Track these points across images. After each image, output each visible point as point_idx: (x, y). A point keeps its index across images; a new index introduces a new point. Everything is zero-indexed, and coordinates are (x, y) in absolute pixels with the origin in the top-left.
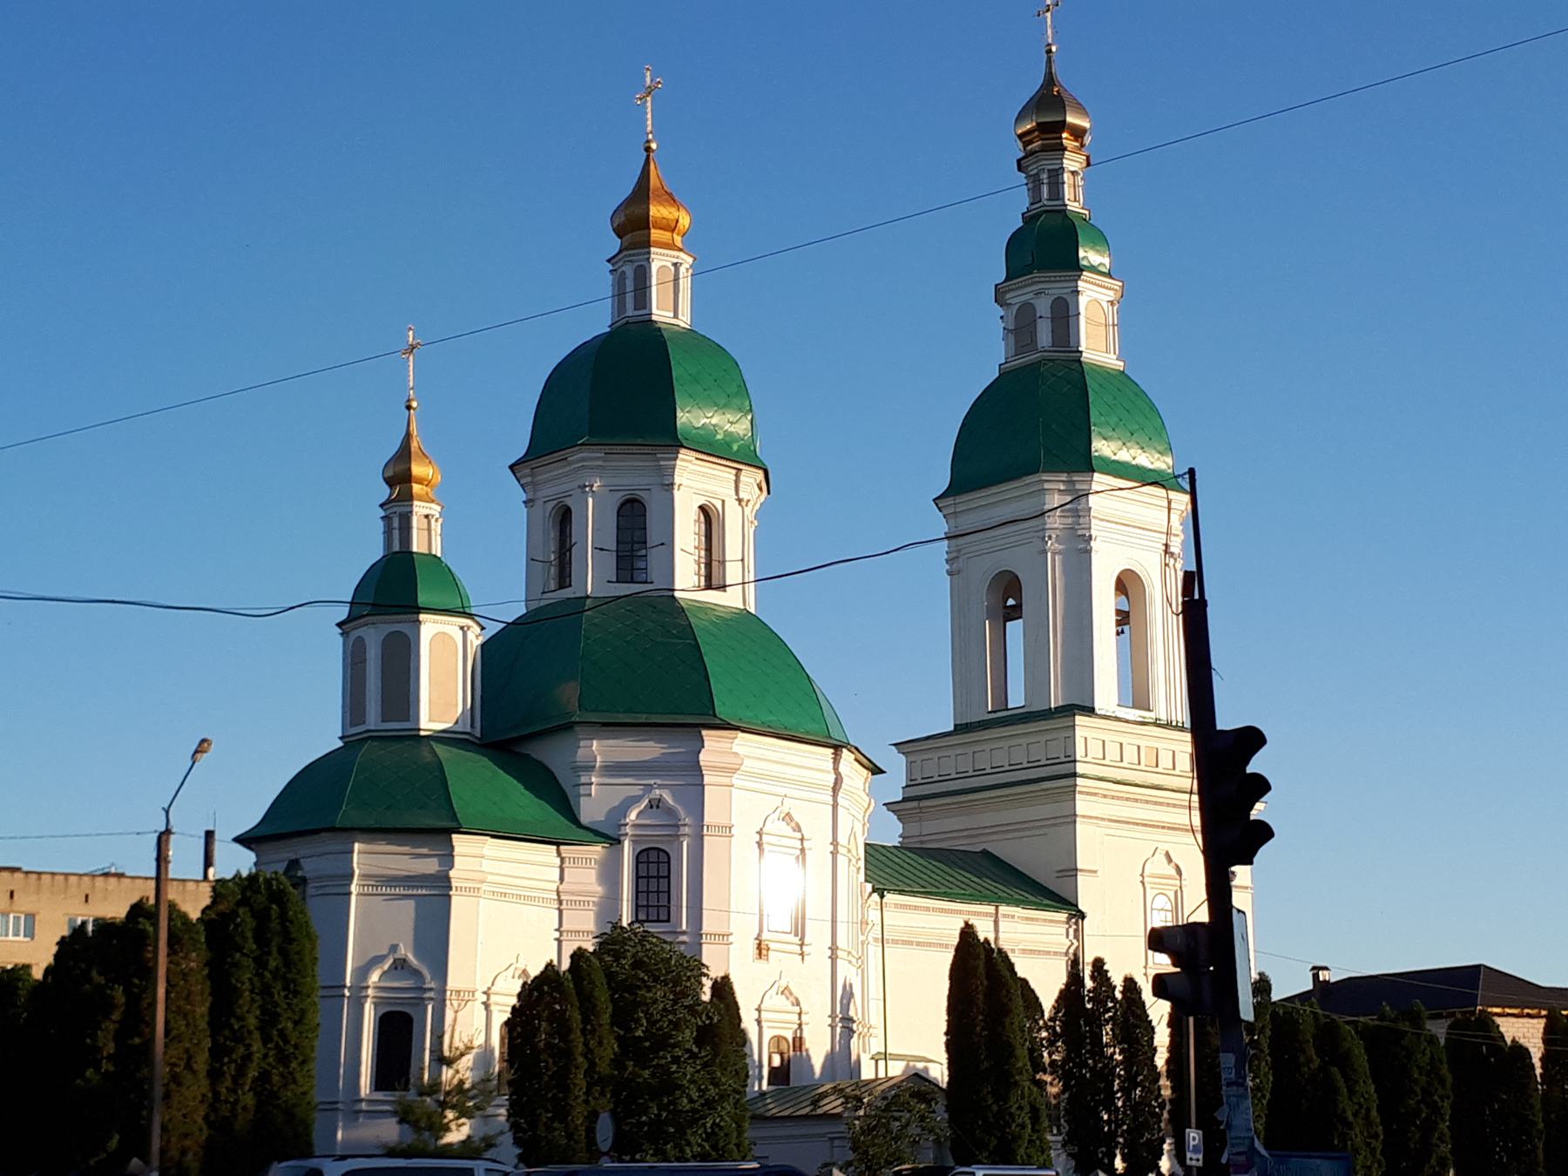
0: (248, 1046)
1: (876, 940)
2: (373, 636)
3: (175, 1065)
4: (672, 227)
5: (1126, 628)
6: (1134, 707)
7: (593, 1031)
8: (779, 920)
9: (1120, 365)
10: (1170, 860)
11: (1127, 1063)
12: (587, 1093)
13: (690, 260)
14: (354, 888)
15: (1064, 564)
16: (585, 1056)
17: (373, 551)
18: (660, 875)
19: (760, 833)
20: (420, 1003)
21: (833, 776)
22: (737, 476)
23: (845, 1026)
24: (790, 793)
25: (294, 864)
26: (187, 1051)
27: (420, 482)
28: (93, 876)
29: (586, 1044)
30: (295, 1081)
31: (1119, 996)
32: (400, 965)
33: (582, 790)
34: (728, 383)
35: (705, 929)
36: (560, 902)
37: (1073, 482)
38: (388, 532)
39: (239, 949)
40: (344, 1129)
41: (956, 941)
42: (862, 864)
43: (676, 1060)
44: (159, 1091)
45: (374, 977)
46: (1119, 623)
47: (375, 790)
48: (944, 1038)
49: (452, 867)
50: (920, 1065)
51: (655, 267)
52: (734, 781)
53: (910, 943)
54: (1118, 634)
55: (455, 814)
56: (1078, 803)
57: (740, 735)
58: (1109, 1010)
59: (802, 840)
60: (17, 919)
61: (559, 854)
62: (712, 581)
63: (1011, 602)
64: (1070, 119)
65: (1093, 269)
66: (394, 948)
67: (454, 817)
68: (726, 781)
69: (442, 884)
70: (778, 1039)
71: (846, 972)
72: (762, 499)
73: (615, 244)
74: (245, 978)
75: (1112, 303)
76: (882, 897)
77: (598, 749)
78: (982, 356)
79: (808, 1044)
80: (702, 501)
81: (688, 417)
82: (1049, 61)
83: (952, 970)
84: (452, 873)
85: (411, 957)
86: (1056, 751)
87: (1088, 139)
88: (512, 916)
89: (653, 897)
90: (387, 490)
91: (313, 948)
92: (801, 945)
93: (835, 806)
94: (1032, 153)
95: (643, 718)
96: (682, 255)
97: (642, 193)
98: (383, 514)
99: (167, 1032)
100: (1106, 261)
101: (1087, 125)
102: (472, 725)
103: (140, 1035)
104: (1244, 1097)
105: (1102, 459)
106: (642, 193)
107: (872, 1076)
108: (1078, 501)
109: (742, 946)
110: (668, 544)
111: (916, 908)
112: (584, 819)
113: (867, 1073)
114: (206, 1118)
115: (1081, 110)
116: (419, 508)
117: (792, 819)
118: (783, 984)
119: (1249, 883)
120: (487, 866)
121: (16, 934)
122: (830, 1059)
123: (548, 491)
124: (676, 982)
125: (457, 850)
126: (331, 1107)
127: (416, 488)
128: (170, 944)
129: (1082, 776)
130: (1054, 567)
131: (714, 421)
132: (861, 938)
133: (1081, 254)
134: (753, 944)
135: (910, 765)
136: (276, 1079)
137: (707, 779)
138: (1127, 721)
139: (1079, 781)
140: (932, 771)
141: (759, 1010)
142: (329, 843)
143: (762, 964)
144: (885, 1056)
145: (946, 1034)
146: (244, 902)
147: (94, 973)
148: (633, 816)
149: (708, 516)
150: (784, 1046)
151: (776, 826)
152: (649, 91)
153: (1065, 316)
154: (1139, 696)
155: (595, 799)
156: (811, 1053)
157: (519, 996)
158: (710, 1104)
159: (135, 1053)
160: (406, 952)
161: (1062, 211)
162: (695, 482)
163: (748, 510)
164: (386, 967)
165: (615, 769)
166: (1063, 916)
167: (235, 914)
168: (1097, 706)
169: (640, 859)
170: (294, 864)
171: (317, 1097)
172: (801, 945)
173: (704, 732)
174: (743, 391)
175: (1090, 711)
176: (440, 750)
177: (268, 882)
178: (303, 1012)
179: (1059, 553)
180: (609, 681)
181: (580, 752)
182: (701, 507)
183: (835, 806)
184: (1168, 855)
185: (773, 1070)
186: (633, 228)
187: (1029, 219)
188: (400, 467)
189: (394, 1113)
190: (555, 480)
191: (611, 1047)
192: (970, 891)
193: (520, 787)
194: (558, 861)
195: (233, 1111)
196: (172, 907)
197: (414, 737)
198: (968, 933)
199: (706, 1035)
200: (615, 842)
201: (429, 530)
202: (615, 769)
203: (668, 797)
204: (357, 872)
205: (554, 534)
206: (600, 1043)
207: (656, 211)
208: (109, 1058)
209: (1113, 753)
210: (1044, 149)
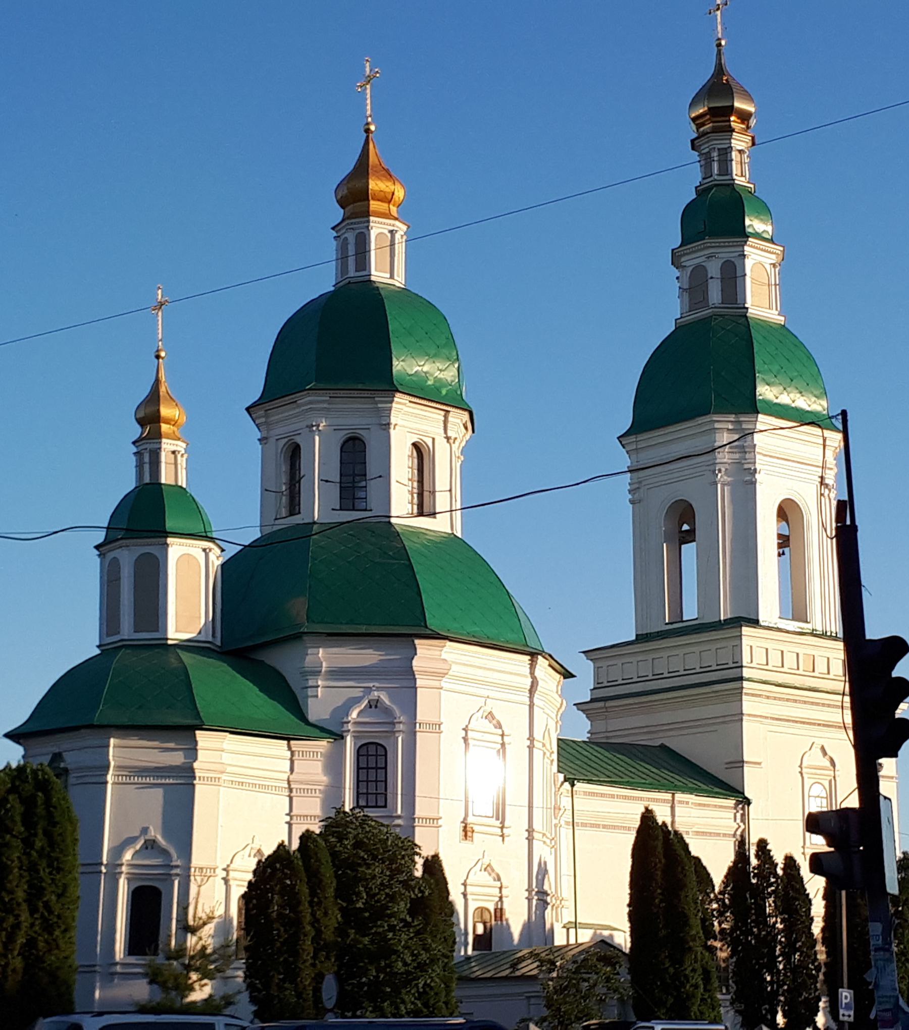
0: (17, 916)
1: (567, 823)
2: (127, 557)
4: (388, 199)
5: (787, 550)
6: (793, 619)
7: (319, 903)
8: (483, 807)
9: (781, 320)
10: (825, 753)
11: (787, 931)
12: (315, 957)
13: (405, 228)
14: (110, 778)
15: (733, 493)
18: (378, 767)
20: (168, 879)
22: (446, 417)
23: (540, 898)
25: (57, 757)
27: (167, 422)
29: (313, 914)
30: (58, 947)
31: (780, 872)
32: (151, 845)
33: (310, 692)
34: (438, 337)
35: (418, 813)
36: (291, 790)
37: (740, 422)
38: (140, 466)
41: (637, 824)
42: (555, 756)
43: (392, 928)
45: (128, 856)
46: (780, 546)
48: (627, 910)
49: (196, 759)
50: (606, 933)
51: (373, 233)
52: (443, 684)
53: (598, 826)
54: (779, 555)
57: (448, 643)
58: (771, 885)
59: (503, 735)
61: (289, 748)
63: (685, 527)
64: (738, 104)
65: (758, 236)
66: (145, 830)
67: (198, 715)
68: (436, 684)
69: (185, 777)
70: (482, 910)
71: (542, 851)
72: (468, 437)
75: (774, 265)
76: (573, 785)
77: (324, 656)
78: (661, 313)
79: (508, 914)
80: (415, 439)
81: (404, 365)
82: (719, 53)
84: (196, 765)
85: (159, 838)
86: (726, 658)
87: (753, 122)
88: (248, 800)
89: (372, 786)
91: (74, 830)
92: (502, 828)
93: (531, 706)
94: (705, 134)
95: (363, 629)
96: (397, 223)
97: (362, 169)
98: (135, 450)
100: (769, 228)
101: (752, 109)
102: (214, 635)
104: (890, 960)
105: (766, 402)
106: (362, 169)
107: (565, 943)
109: (450, 829)
110: (385, 476)
111: (602, 795)
112: (312, 718)
113: (560, 940)
116: (167, 445)
117: (493, 718)
118: (486, 861)
119: (894, 774)
120: (226, 758)
122: (528, 927)
123: (280, 430)
124: (393, 860)
125: (200, 744)
126: (90, 970)
127: (164, 427)
129: (748, 680)
131: (425, 369)
132: (555, 821)
133: (747, 222)
135: (597, 670)
136: (41, 945)
138: (788, 632)
139: (745, 684)
140: (616, 675)
141: (465, 885)
142: (90, 738)
143: (467, 844)
144: (575, 925)
146: (13, 790)
148: (354, 714)
150: (487, 917)
152: (369, 79)
153: (733, 277)
155: (321, 700)
156: (511, 922)
160: (155, 833)
162: (409, 422)
164: (138, 847)
166: (731, 802)
168: (761, 618)
169: (360, 752)
170: (57, 757)
171: (77, 960)
172: (502, 828)
173: (417, 642)
174: (451, 341)
175: (754, 622)
176: (186, 657)
178: (65, 887)
179: (728, 484)
180: (335, 596)
181: (308, 658)
182: (415, 445)
183: (531, 706)
185: (477, 938)
186: (355, 200)
187: (702, 192)
188: (150, 409)
189: (145, 975)
190: (287, 421)
191: (335, 917)
193: (256, 689)
194: (288, 754)
198: (648, 817)
199: (419, 907)
200: (339, 737)
201: (176, 464)
204: (112, 764)
205: (285, 468)
206: (326, 914)
207: (375, 185)
210: (714, 130)
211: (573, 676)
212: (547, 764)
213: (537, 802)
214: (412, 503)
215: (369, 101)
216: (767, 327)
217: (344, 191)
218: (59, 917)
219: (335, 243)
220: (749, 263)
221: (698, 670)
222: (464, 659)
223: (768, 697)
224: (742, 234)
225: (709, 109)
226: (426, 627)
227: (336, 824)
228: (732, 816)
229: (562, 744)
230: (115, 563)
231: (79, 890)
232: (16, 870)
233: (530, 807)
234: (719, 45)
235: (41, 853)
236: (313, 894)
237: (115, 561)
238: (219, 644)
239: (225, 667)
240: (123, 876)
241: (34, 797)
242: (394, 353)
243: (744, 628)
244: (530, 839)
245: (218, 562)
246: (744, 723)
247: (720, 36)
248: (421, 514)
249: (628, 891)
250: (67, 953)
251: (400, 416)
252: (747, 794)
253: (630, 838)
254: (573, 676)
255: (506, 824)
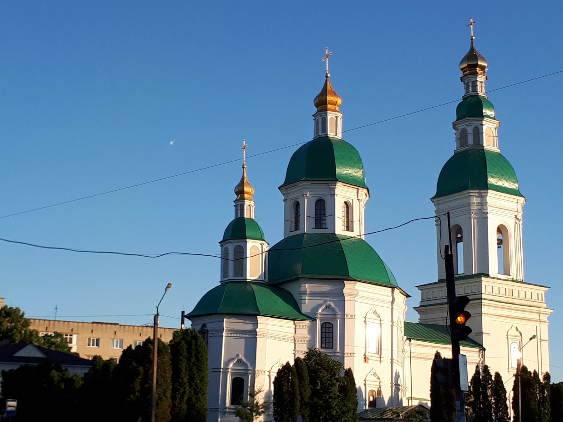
0: (184, 388)
1: (408, 356)
2: (231, 247)
3: (160, 394)
4: (335, 104)
5: (501, 245)
6: (505, 274)
7: (303, 387)
8: (372, 349)
9: (498, 151)
10: (517, 330)
11: (496, 403)
12: (301, 408)
13: (341, 115)
14: (224, 334)
15: (477, 222)
16: (300, 395)
17: (232, 217)
18: (330, 332)
19: (365, 318)
20: (247, 375)
21: (391, 298)
22: (358, 191)
23: (397, 387)
24: (376, 303)
25: (204, 325)
26: (164, 389)
27: (247, 193)
28: (142, 327)
29: (300, 391)
30: (200, 401)
31: (493, 379)
32: (240, 361)
33: (303, 301)
34: (355, 159)
35: (346, 351)
36: (295, 341)
37: (481, 193)
38: (236, 211)
39: (182, 355)
40: (221, 418)
41: (433, 357)
42: (403, 329)
43: (331, 397)
44: (154, 403)
45: (231, 365)
46: (498, 244)
47: (231, 300)
48: (430, 392)
49: (257, 327)
50: (424, 402)
51: (329, 118)
52: (356, 299)
53: (421, 358)
54: (498, 248)
55: (258, 309)
56: (483, 309)
57: (358, 283)
58: (490, 384)
59: (380, 320)
60: (117, 341)
61: (294, 324)
62: (349, 226)
63: (459, 236)
64: (479, 63)
65: (488, 117)
66: (238, 355)
67: (258, 310)
68: (353, 299)
69: (254, 333)
70: (372, 391)
71: (397, 368)
72: (367, 199)
73: (315, 110)
74: (183, 365)
75: (495, 128)
76: (410, 341)
77: (308, 287)
78: (448, 148)
79: (383, 393)
80: (345, 200)
81: (340, 171)
82: (472, 42)
83: (432, 368)
84: (257, 330)
85: (243, 358)
86: (475, 290)
87: (486, 70)
88: (278, 344)
89: (327, 339)
90: (236, 196)
91: (207, 355)
92: (380, 358)
93: (392, 309)
94: (466, 75)
95: (324, 276)
96: (338, 113)
97: (324, 92)
98: (234, 204)
99: (157, 383)
100: (493, 114)
101: (486, 65)
102: (265, 278)
103: (148, 384)
104: (463, 415)
105: (492, 185)
106: (324, 92)
107: (407, 405)
108: (483, 198)
109: (359, 358)
110: (333, 215)
111: (423, 345)
112: (303, 311)
113: (405, 404)
114: (171, 413)
115: (484, 60)
116: (247, 203)
117: (377, 313)
118: (374, 371)
119: (547, 339)
120: (269, 327)
121: (117, 346)
122: (391, 399)
123: (292, 196)
124: (332, 370)
125: (259, 322)
126: (216, 410)
127: (246, 195)
128: (158, 353)
129: (484, 299)
130: (474, 223)
131: (349, 172)
132: (403, 356)
133: (484, 111)
134: (363, 357)
135: (422, 294)
136: (194, 399)
137: (346, 298)
138: (501, 280)
139: (483, 301)
140: (430, 296)
141: (365, 380)
142: (216, 318)
143: (366, 364)
144: (412, 398)
145: (431, 391)
146: (183, 339)
147: (133, 363)
148: (320, 311)
149: (348, 206)
150: (374, 394)
151: (371, 315)
152: (327, 56)
153: (478, 133)
154: (505, 269)
155: (307, 304)
156: (384, 396)
157: (277, 373)
158: (343, 413)
159: (147, 390)
160: (242, 357)
161: (477, 96)
162: (343, 193)
163: (362, 203)
164: (235, 362)
165: (313, 294)
166: (477, 350)
167: (180, 343)
168: (490, 274)
169: (322, 326)
170: (204, 325)
171: (207, 406)
172: (380, 358)
173: (345, 282)
174: (360, 161)
175: (487, 275)
176: (254, 287)
177: (192, 332)
178: (203, 377)
179: (476, 218)
180: (313, 264)
181: (302, 288)
182: (345, 203)
183: (392, 309)
184: (516, 328)
185: (370, 402)
186: (322, 104)
187: (465, 99)
188: (240, 188)
189: (235, 413)
190: (294, 193)
191: (308, 393)
192: (438, 339)
193: (281, 300)
194: (294, 326)
195: (180, 410)
196: (159, 340)
197: (245, 282)
198: (438, 355)
199: (343, 389)
200: (314, 320)
201: (250, 210)
202: (313, 294)
203: (332, 305)
204: (225, 328)
205: (293, 211)
206: (305, 391)
207: (329, 98)
208: (138, 391)
209: (496, 291)
210: (470, 74)
211: (410, 297)
212: (399, 332)
213: (395, 348)
214: (344, 226)
215: (327, 65)
216: (492, 153)
217: (317, 101)
218: (201, 389)
219: (313, 121)
220: (484, 128)
221: (471, 294)
222: (365, 289)
223: (493, 307)
224: (482, 116)
225: (468, 65)
226: (349, 276)
227: (311, 353)
228: (478, 355)
229: (406, 324)
230: (227, 249)
231: (209, 378)
232: (184, 370)
233: (392, 351)
234: (472, 39)
235: (194, 364)
236: (300, 383)
237: (227, 248)
238: (267, 281)
239: (269, 291)
240: (229, 373)
241: (191, 342)
242: (337, 166)
243: (483, 278)
244: (392, 363)
245: (267, 249)
246: (483, 317)
247: (472, 35)
248: (348, 230)
249: (430, 385)
250: (204, 403)
251: (339, 191)
252: (484, 346)
253: (430, 363)
254: (410, 297)
255: (382, 356)
